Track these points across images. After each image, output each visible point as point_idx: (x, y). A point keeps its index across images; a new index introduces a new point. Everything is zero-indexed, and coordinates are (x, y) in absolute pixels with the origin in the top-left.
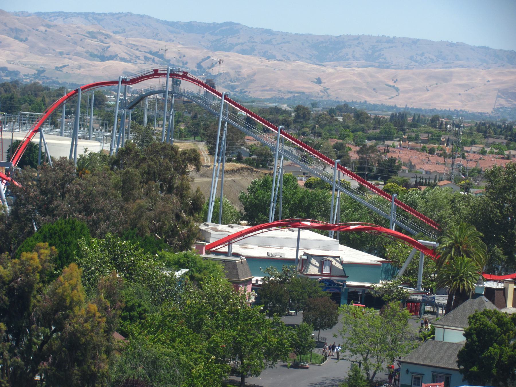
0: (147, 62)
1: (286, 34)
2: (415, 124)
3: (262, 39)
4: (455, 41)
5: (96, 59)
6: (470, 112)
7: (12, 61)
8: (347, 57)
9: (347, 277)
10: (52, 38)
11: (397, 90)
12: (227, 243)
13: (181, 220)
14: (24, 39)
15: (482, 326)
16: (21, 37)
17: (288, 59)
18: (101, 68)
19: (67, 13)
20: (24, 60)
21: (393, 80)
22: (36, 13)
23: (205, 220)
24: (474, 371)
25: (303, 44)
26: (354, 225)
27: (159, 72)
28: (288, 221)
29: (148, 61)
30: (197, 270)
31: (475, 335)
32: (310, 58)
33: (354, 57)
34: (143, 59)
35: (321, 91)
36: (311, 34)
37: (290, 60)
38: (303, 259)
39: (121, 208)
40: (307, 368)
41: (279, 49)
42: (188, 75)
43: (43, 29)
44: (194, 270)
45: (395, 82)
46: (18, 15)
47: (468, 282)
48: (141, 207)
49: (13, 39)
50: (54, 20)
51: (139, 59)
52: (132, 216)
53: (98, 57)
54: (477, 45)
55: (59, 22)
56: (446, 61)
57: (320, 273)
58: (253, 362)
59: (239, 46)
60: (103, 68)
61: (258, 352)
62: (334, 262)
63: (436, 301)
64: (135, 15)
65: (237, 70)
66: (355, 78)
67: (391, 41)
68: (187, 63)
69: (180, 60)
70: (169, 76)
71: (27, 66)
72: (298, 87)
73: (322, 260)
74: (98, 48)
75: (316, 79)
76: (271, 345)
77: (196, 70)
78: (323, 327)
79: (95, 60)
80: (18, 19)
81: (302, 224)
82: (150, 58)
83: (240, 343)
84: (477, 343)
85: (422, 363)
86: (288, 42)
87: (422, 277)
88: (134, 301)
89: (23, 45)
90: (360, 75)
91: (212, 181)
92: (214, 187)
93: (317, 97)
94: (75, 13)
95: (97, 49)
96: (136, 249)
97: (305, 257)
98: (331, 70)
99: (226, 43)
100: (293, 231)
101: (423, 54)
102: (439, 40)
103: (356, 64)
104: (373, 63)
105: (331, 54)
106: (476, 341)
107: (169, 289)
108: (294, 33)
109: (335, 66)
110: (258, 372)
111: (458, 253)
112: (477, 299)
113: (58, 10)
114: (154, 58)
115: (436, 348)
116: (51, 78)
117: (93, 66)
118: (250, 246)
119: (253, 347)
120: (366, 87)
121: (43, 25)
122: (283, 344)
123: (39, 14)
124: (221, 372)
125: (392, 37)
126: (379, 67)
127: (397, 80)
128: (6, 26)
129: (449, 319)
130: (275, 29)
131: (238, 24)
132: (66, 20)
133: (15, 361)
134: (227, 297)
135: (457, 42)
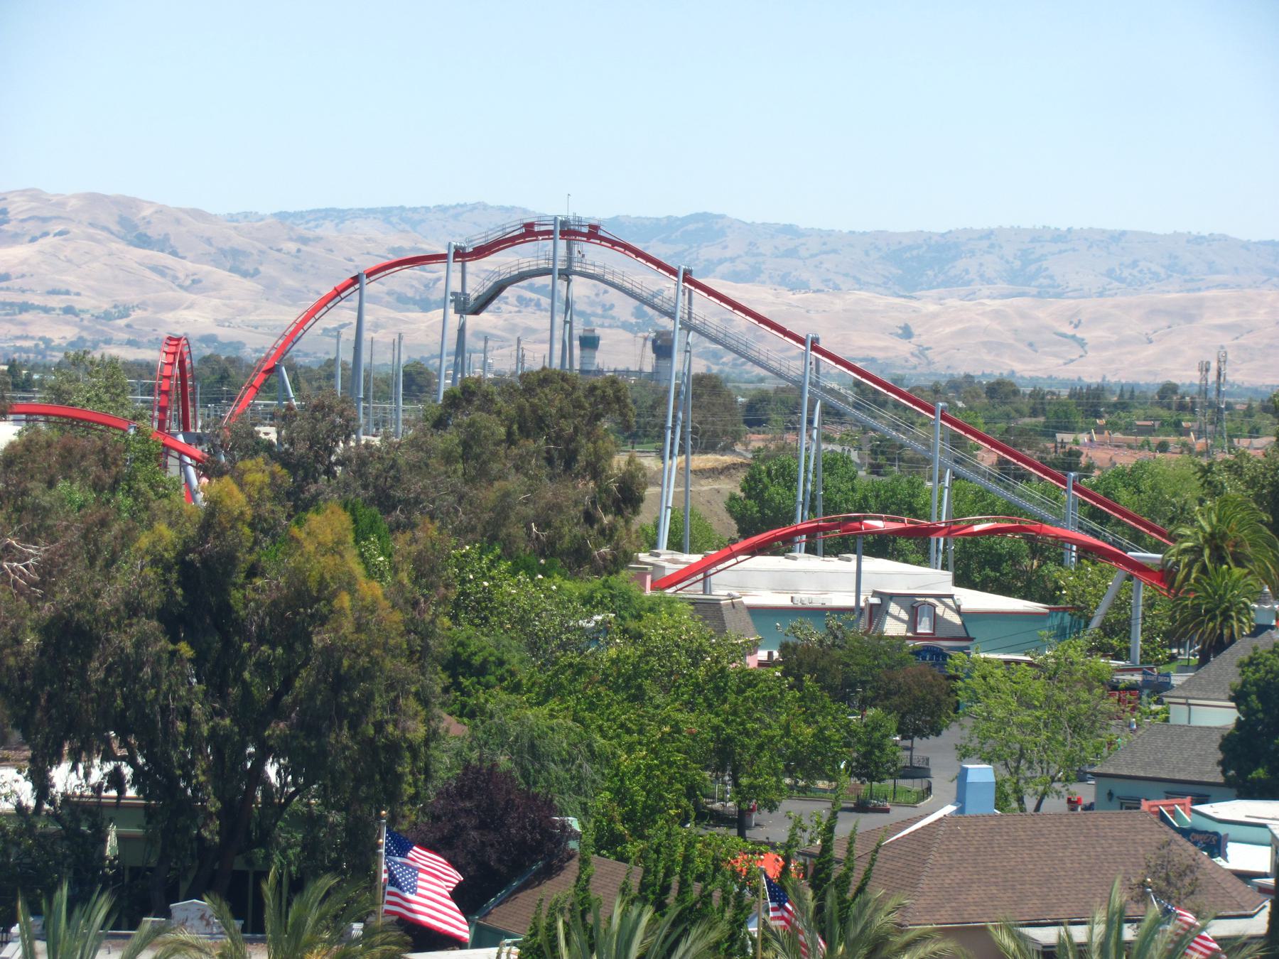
0: (523, 310)
1: (830, 233)
2: (1122, 406)
3: (776, 247)
4: (1205, 233)
5: (412, 307)
6: (1246, 385)
7: (226, 320)
8: (966, 277)
9: (972, 639)
10: (312, 266)
11: (1082, 343)
12: (701, 576)
13: (596, 527)
14: (252, 271)
15: (1270, 676)
16: (244, 267)
17: (837, 288)
18: (423, 326)
19: (343, 211)
20: (254, 318)
21: (1071, 323)
22: (275, 215)
23: (653, 545)
24: (1259, 779)
25: (867, 254)
26: (979, 522)
27: (536, 229)
28: (833, 520)
29: (527, 306)
30: (632, 616)
31: (1254, 697)
32: (884, 283)
33: (981, 276)
34: (516, 303)
35: (912, 354)
36: (882, 231)
37: (840, 289)
38: (872, 606)
39: (461, 498)
40: (887, 811)
41: (816, 266)
42: (601, 233)
43: (292, 247)
44: (626, 615)
45: (1076, 326)
46: (237, 221)
47: (1240, 621)
48: (507, 494)
49: (227, 273)
50: (317, 226)
51: (506, 303)
52: (486, 516)
53: (415, 302)
54: (1255, 239)
55: (327, 230)
56: (1187, 277)
57: (909, 634)
58: (760, 780)
59: (727, 264)
60: (428, 327)
61: (772, 757)
62: (940, 610)
63: (1172, 682)
64: (492, 207)
65: (724, 317)
66: (986, 322)
67: (1060, 237)
68: (612, 307)
69: (597, 300)
70: (558, 236)
71: (260, 330)
72: (861, 348)
73: (914, 606)
74: (415, 283)
75: (900, 328)
76: (799, 742)
77: (633, 320)
78: (920, 733)
79: (408, 310)
80: (235, 228)
81: (866, 525)
82: (531, 300)
83: (730, 739)
84: (1261, 715)
85: (1142, 774)
86: (835, 251)
87: (1140, 638)
88: (485, 653)
89: (248, 283)
90: (997, 314)
91: (664, 468)
92: (669, 479)
93: (903, 367)
94: (362, 210)
95: (412, 286)
96: (492, 564)
97: (876, 601)
98: (932, 308)
99: (697, 259)
100: (849, 560)
101: (1135, 264)
102: (1169, 231)
103: (987, 292)
104: (1027, 289)
105: (930, 273)
106: (1258, 711)
107: (568, 638)
108: (845, 230)
109: (941, 299)
110: (772, 801)
111: (1219, 558)
112: (1260, 637)
113: (322, 206)
114: (539, 300)
115: (1172, 740)
116: (315, 353)
117: (405, 322)
118: (754, 593)
119: (761, 747)
120: (1011, 341)
121: (291, 239)
122: (827, 740)
123: (282, 216)
124: (685, 759)
125: (1064, 228)
126: (1039, 295)
127: (1080, 321)
128: (211, 244)
129: (1201, 684)
130: (803, 223)
131: (722, 217)
132: (341, 226)
133: (218, 724)
134: (698, 652)
135: (1211, 235)
